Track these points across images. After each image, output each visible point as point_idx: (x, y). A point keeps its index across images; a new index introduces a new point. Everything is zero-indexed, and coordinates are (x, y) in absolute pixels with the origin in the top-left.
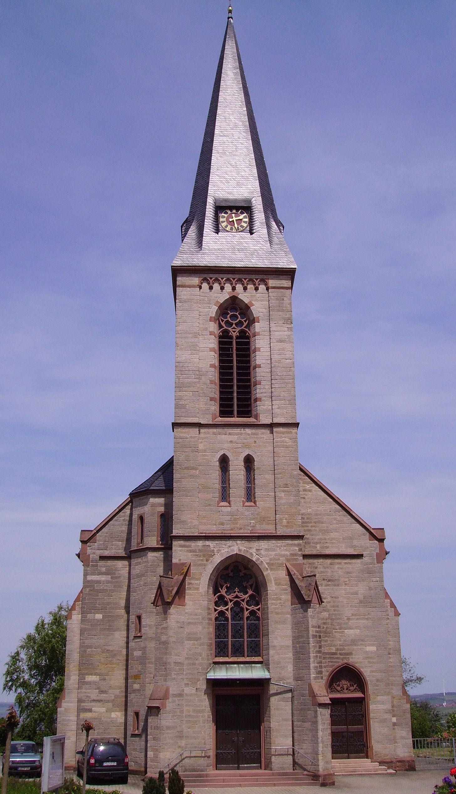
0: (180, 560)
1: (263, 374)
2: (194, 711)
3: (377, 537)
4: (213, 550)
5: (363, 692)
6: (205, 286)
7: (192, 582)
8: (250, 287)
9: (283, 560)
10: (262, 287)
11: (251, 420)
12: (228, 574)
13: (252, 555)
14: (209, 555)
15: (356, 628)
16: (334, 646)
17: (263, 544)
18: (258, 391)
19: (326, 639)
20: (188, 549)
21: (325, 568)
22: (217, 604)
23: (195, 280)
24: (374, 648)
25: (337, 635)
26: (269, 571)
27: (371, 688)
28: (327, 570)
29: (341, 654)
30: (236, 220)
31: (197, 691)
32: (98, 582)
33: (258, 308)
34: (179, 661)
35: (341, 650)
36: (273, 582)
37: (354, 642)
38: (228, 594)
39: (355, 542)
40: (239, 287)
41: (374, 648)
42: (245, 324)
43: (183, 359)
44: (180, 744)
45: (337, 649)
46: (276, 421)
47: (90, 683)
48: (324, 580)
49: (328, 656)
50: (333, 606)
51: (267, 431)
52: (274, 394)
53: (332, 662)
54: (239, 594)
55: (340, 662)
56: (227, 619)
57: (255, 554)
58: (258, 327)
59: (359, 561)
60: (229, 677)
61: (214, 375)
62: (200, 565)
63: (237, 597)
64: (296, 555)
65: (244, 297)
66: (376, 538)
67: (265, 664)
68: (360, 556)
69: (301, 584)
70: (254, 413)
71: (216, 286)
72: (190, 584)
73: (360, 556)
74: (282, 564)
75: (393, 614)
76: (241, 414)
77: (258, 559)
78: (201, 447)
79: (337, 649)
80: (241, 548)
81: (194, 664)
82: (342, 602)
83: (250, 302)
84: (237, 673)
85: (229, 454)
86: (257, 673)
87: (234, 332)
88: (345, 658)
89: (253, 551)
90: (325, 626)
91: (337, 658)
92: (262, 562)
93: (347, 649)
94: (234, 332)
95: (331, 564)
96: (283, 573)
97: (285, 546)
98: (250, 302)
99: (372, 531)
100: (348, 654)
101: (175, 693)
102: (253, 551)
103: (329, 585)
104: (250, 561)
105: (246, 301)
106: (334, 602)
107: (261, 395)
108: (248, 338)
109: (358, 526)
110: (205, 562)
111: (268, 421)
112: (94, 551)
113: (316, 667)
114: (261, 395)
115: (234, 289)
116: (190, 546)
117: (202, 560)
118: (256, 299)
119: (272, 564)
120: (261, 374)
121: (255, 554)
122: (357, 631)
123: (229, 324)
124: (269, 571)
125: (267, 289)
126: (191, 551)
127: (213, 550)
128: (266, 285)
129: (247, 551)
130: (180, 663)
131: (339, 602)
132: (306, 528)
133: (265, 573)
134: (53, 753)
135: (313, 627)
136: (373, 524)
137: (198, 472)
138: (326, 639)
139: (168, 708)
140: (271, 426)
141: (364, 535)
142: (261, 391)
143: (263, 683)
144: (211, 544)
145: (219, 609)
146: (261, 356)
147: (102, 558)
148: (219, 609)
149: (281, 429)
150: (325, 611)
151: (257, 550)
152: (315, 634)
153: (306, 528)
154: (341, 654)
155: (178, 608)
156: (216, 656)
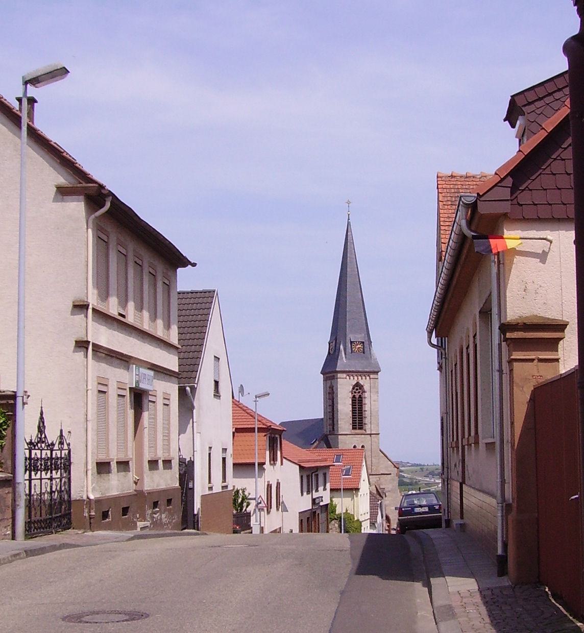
5: (389, 523)
6: (348, 377)
8: (364, 378)
10: (368, 378)
23: (344, 375)
27: (392, 522)
30: (258, 428)
33: (366, 388)
39: (389, 469)
40: (360, 378)
43: (375, 530)
46: (372, 432)
51: (369, 436)
58: (366, 395)
59: (390, 476)
65: (361, 382)
68: (390, 474)
70: (364, 428)
71: (352, 378)
73: (390, 474)
76: (360, 429)
78: (347, 442)
87: (357, 396)
94: (357, 396)
105: (362, 384)
109: (390, 462)
111: (369, 433)
115: (358, 379)
118: (365, 382)
120: (367, 414)
123: (355, 392)
125: (370, 379)
128: (370, 377)
134: (302, 520)
140: (371, 434)
142: (367, 421)
146: (367, 408)
149: (374, 436)
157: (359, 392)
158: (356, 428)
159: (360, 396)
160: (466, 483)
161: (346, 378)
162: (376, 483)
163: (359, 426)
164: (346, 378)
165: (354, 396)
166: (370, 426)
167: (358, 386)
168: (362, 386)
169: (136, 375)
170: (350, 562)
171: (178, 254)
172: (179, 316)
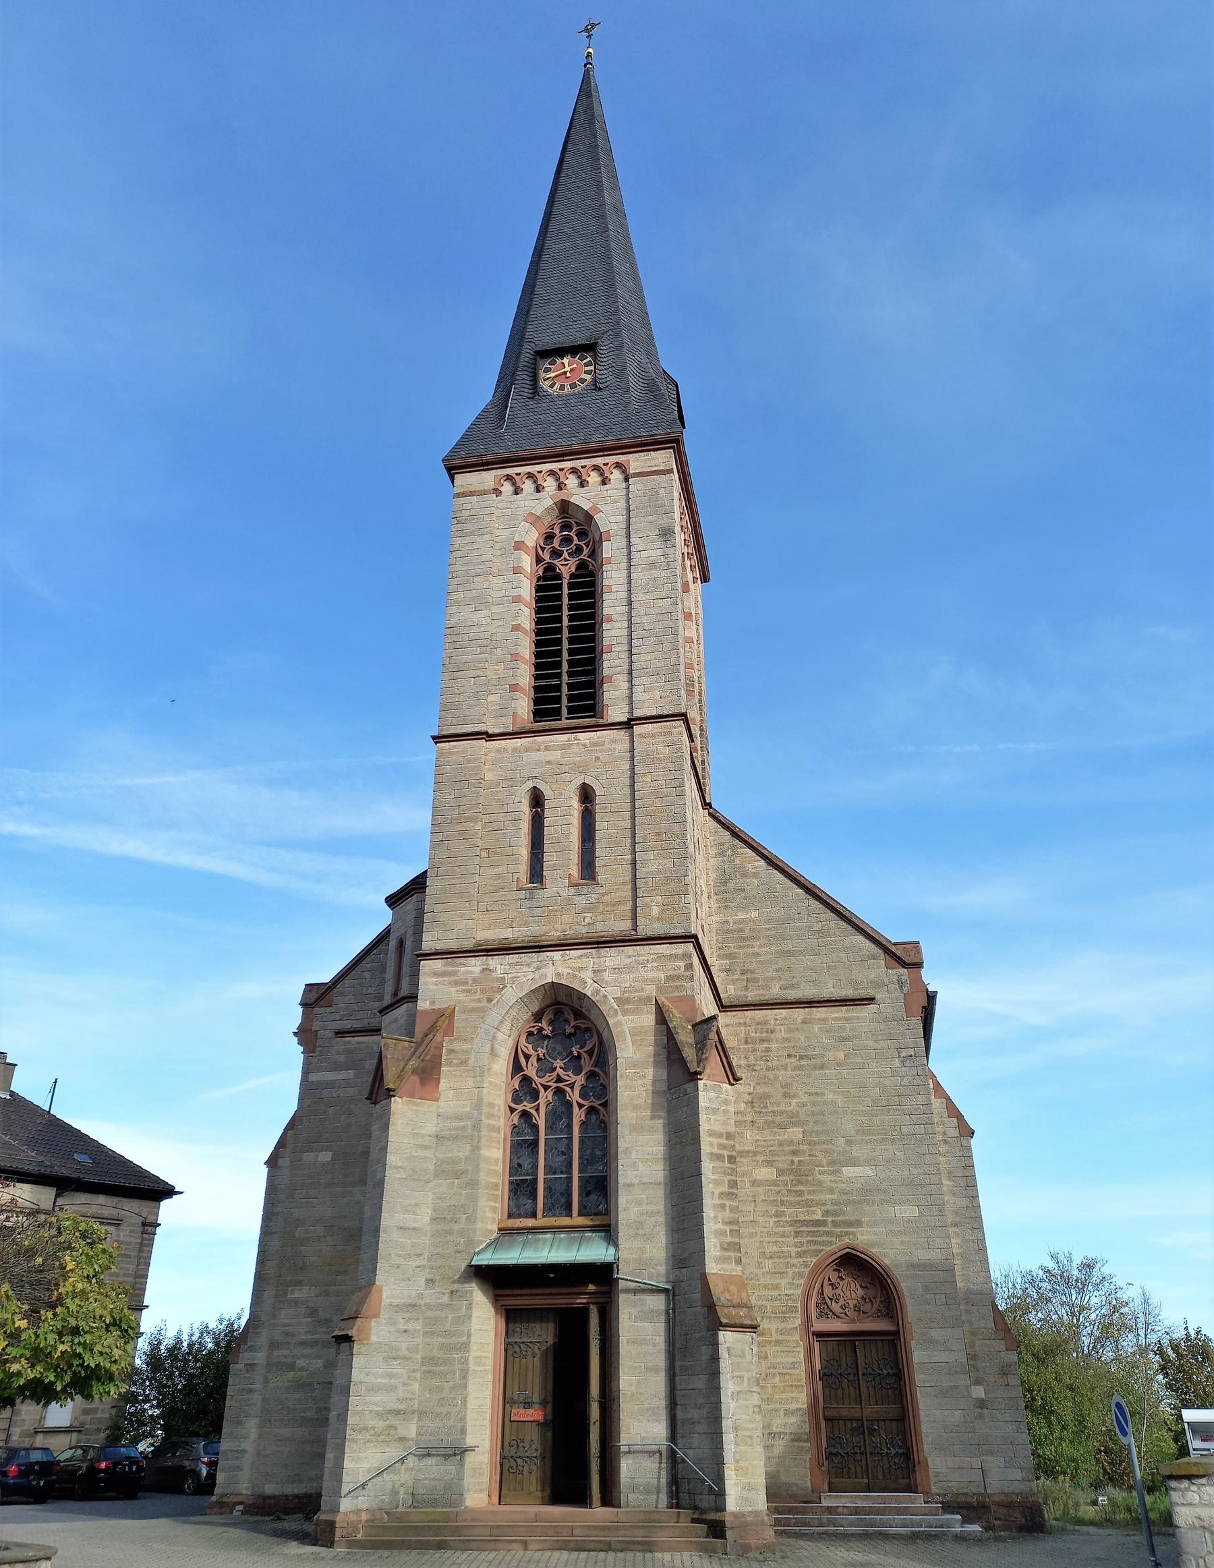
0: (433, 1003)
1: (614, 633)
2: (443, 1347)
3: (905, 959)
4: (503, 978)
6: (507, 488)
7: (457, 1046)
9: (651, 990)
11: (601, 721)
12: (541, 1030)
13: (584, 982)
14: (492, 989)
15: (868, 1162)
16: (822, 1204)
17: (611, 958)
18: (606, 664)
19: (800, 1188)
20: (452, 979)
21: (791, 1031)
22: (517, 1099)
23: (487, 478)
24: (911, 1211)
25: (826, 1179)
26: (620, 1017)
28: (797, 1035)
29: (834, 1224)
31: (451, 1299)
32: (332, 1085)
33: (608, 519)
34: (415, 1225)
35: (836, 1213)
36: (629, 1039)
37: (866, 1193)
38: (541, 1074)
41: (911, 1211)
42: (586, 551)
44: (402, 1432)
45: (827, 1213)
47: (296, 1302)
48: (789, 1056)
49: (804, 1229)
50: (813, 1114)
51: (622, 734)
52: (635, 666)
53: (815, 1243)
54: (533, 1060)
55: (836, 1245)
56: (535, 1127)
57: (590, 982)
60: (521, 1261)
61: (526, 648)
62: (473, 1010)
63: (559, 1079)
64: (678, 977)
65: (581, 499)
66: (903, 964)
67: (608, 1231)
69: (685, 1037)
72: (451, 1051)
74: (648, 999)
75: (954, 1132)
77: (598, 991)
79: (827, 1213)
80: (561, 970)
81: (450, 1232)
82: (833, 1103)
83: (594, 507)
84: (545, 1253)
85: (541, 786)
86: (593, 1251)
87: (567, 568)
88: (847, 1233)
89: (587, 975)
90: (796, 1159)
91: (827, 1233)
92: (605, 996)
93: (850, 1213)
95: (804, 1022)
96: (648, 1020)
97: (654, 961)
98: (594, 507)
99: (893, 949)
100: (851, 1224)
101: (396, 1301)
102: (587, 975)
103: (801, 1067)
104: (582, 997)
105: (586, 506)
106: (814, 1104)
107: (611, 671)
108: (592, 574)
109: (860, 939)
110: (485, 1004)
112: (329, 1021)
113: (722, 1233)
114: (611, 671)
115: (561, 486)
116: (454, 973)
117: (479, 1001)
119: (627, 1001)
121: (590, 982)
122: (868, 1171)
124: (620, 1017)
125: (627, 479)
126: (456, 983)
127: (503, 978)
129: (575, 976)
130: (414, 1229)
131: (825, 1103)
132: (748, 950)
133: (611, 1021)
135: (712, 1134)
136: (894, 935)
137: (479, 826)
138: (800, 1188)
139: (374, 1338)
141: (874, 957)
142: (612, 663)
143: (603, 1274)
144: (497, 964)
145: (520, 1108)
147: (340, 1033)
148: (520, 1108)
150: (794, 1124)
151: (594, 971)
152: (716, 1151)
153: (748, 950)
154: (834, 1224)
155: (417, 1105)
156: (510, 1216)
157: (579, 550)
158: (556, 713)
159: (582, 565)
160: (724, 1321)
161: (497, 492)
162: (660, 989)
163: (570, 674)
164: (497, 492)
165: (550, 568)
166: (625, 685)
167: (574, 528)
168: (589, 517)
169: (572, 1528)
170: (395, 1236)
171: (276, 1243)
172: (331, 1383)
